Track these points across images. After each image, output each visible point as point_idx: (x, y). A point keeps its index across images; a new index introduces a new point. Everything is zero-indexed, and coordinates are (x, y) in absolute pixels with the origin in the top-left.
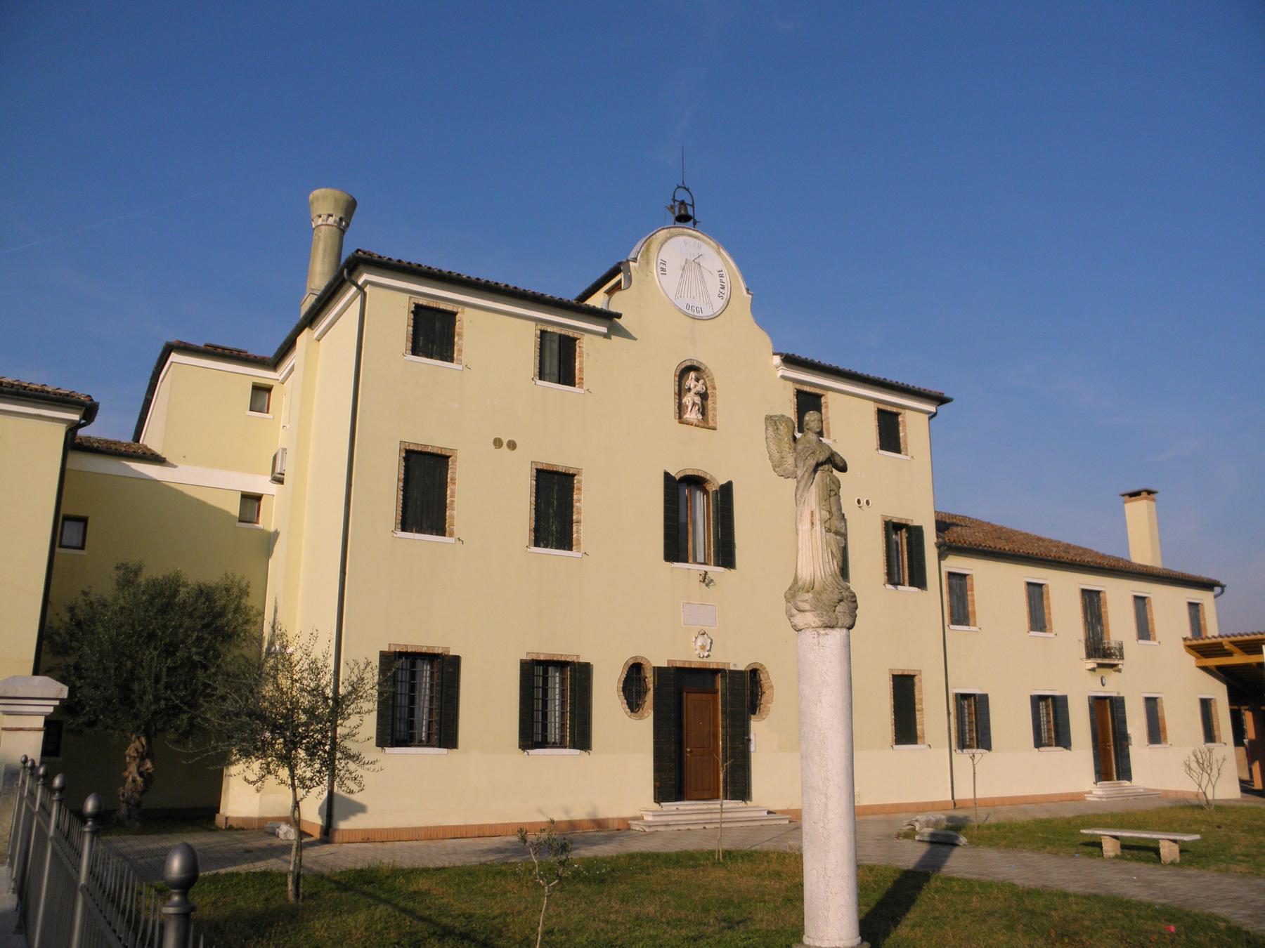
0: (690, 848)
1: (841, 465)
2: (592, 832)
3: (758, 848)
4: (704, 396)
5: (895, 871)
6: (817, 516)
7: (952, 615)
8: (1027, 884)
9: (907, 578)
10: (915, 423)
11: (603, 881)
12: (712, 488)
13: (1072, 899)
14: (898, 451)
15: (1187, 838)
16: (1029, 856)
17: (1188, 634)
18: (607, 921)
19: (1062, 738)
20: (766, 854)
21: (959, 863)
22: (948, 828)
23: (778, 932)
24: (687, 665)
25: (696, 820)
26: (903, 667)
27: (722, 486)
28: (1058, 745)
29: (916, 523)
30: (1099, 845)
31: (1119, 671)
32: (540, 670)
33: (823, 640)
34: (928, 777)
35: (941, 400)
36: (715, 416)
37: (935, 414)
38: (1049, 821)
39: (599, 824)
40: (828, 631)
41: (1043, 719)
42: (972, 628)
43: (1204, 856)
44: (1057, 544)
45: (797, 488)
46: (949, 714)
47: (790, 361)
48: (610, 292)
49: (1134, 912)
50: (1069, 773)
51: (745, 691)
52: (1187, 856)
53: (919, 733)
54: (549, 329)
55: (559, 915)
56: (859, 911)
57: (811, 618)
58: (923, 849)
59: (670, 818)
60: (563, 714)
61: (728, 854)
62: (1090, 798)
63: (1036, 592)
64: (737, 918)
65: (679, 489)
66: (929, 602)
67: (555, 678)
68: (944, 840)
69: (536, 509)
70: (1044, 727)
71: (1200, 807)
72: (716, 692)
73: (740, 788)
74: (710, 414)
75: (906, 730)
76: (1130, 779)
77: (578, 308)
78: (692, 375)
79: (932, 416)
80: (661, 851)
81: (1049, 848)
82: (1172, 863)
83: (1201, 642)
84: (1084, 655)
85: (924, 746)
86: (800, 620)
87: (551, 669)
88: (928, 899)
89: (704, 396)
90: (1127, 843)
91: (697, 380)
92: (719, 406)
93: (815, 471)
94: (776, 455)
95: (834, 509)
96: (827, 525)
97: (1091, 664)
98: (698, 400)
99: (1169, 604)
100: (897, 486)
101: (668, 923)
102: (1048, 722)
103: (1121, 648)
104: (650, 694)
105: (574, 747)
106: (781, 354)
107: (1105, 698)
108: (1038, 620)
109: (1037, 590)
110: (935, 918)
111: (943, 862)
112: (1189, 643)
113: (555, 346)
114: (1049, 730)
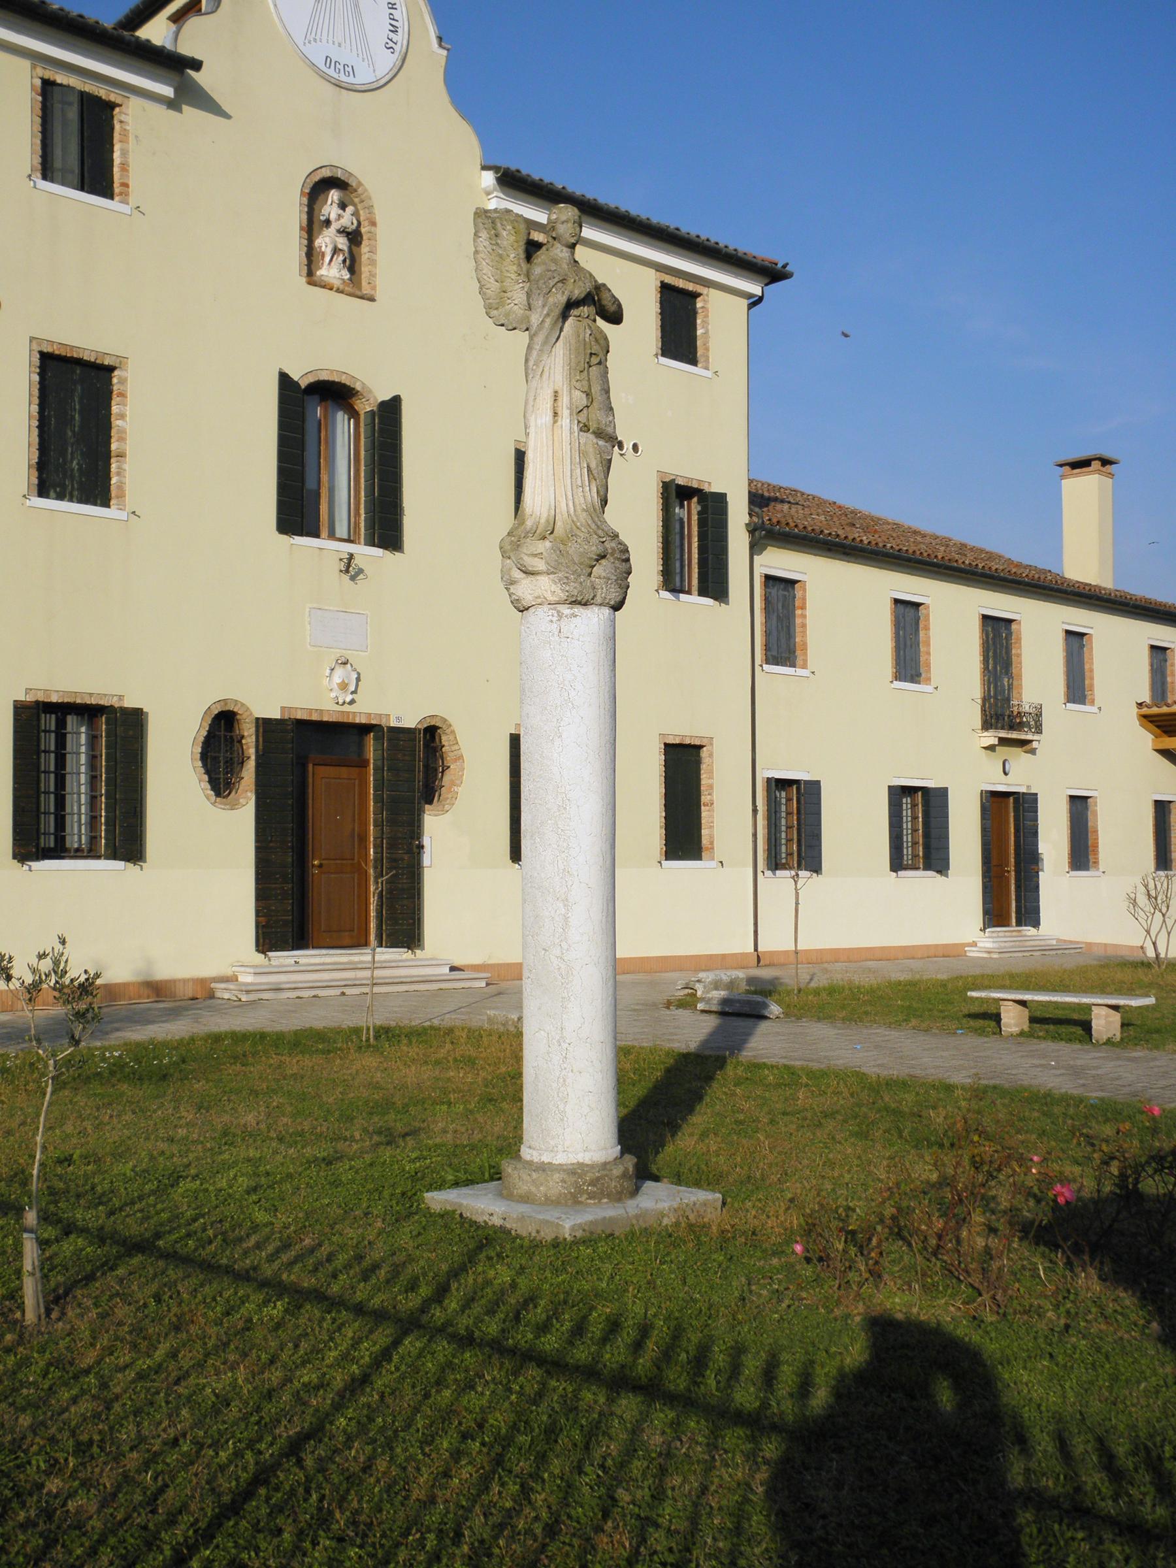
0: (319, 1025)
1: (612, 308)
2: (146, 1002)
3: (436, 1022)
4: (354, 237)
5: (668, 1054)
6: (564, 400)
7: (767, 648)
8: (884, 1073)
9: (695, 582)
10: (723, 315)
11: (164, 1077)
12: (365, 406)
13: (958, 1093)
14: (693, 361)
15: (1135, 1003)
16: (881, 1033)
17: (1146, 697)
18: (171, 1140)
19: (934, 857)
20: (450, 1031)
21: (768, 1043)
22: (748, 992)
23: (473, 1147)
24: (315, 717)
25: (325, 979)
26: (684, 731)
27: (383, 404)
28: (927, 867)
29: (715, 489)
30: (997, 1018)
31: (1033, 752)
32: (51, 721)
33: (568, 626)
34: (719, 914)
35: (772, 274)
36: (373, 275)
37: (761, 299)
38: (913, 983)
39: (158, 989)
40: (578, 610)
41: (907, 826)
42: (800, 672)
43: (1158, 1031)
44: (946, 542)
45: (530, 348)
46: (755, 811)
47: (513, 181)
48: (178, 18)
49: (1056, 1110)
50: (942, 914)
51: (416, 762)
52: (1132, 1031)
53: (705, 841)
54: (61, 78)
55: (83, 1133)
56: (620, 1104)
57: (546, 587)
58: (711, 1022)
59: (282, 978)
60: (93, 800)
61: (385, 1033)
62: (972, 953)
63: (907, 614)
64: (399, 1127)
65: (308, 404)
66: (735, 620)
67: (79, 736)
68: (743, 1009)
69: (41, 427)
70: (907, 838)
71: (1146, 965)
72: (364, 764)
73: (404, 926)
74: (365, 270)
75: (683, 836)
76: (1036, 924)
77: (121, 42)
78: (334, 195)
79: (756, 302)
80: (269, 1029)
81: (914, 1022)
82: (1109, 1042)
83: (1165, 710)
84: (977, 721)
85: (713, 864)
86: (526, 589)
87: (71, 720)
88: (721, 1094)
89: (354, 237)
90: (1038, 1014)
91: (343, 206)
92: (381, 256)
93: (564, 316)
94: (494, 286)
95: (596, 389)
96: (583, 417)
97: (990, 738)
98: (342, 243)
99: (1121, 646)
100: (696, 421)
101: (281, 1140)
102: (915, 830)
103: (1039, 715)
104: (251, 765)
105: (114, 855)
106: (495, 169)
107: (1006, 795)
108: (909, 663)
109: (910, 611)
110: (739, 1122)
111: (745, 1041)
112: (1145, 711)
113: (73, 114)
114: (915, 843)
